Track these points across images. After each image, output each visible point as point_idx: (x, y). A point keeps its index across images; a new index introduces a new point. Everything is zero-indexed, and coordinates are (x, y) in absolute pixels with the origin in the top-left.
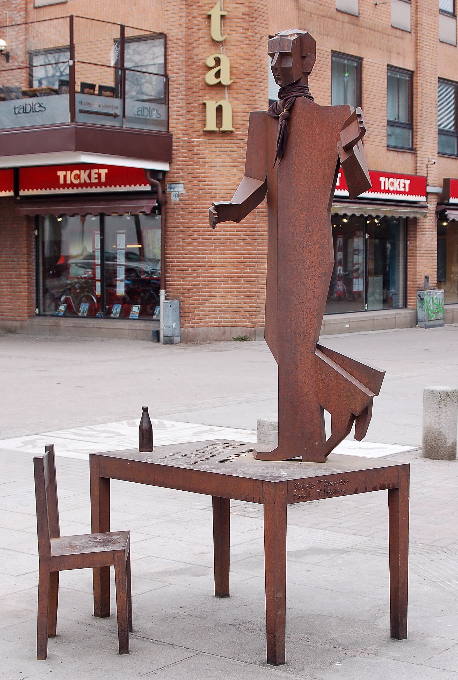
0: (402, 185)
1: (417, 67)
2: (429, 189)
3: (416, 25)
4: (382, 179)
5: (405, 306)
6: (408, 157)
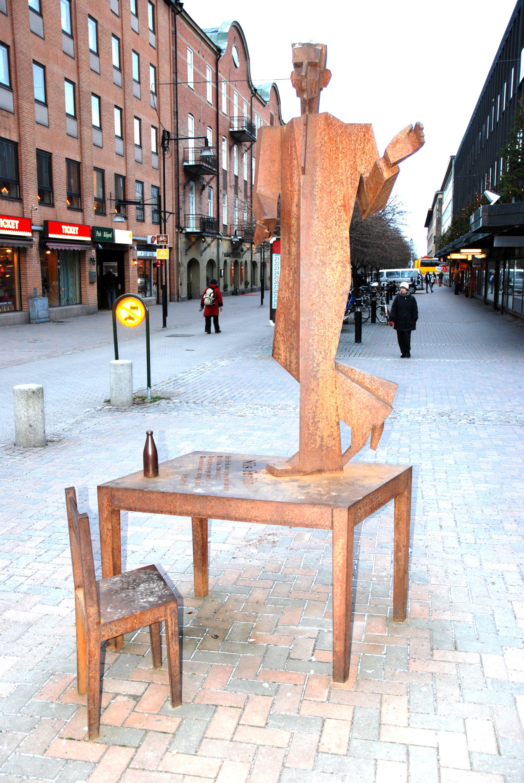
0: (13, 224)
1: (20, 140)
2: (33, 228)
3: (18, 107)
4: (63, 227)
5: (21, 310)
6: (17, 205)
